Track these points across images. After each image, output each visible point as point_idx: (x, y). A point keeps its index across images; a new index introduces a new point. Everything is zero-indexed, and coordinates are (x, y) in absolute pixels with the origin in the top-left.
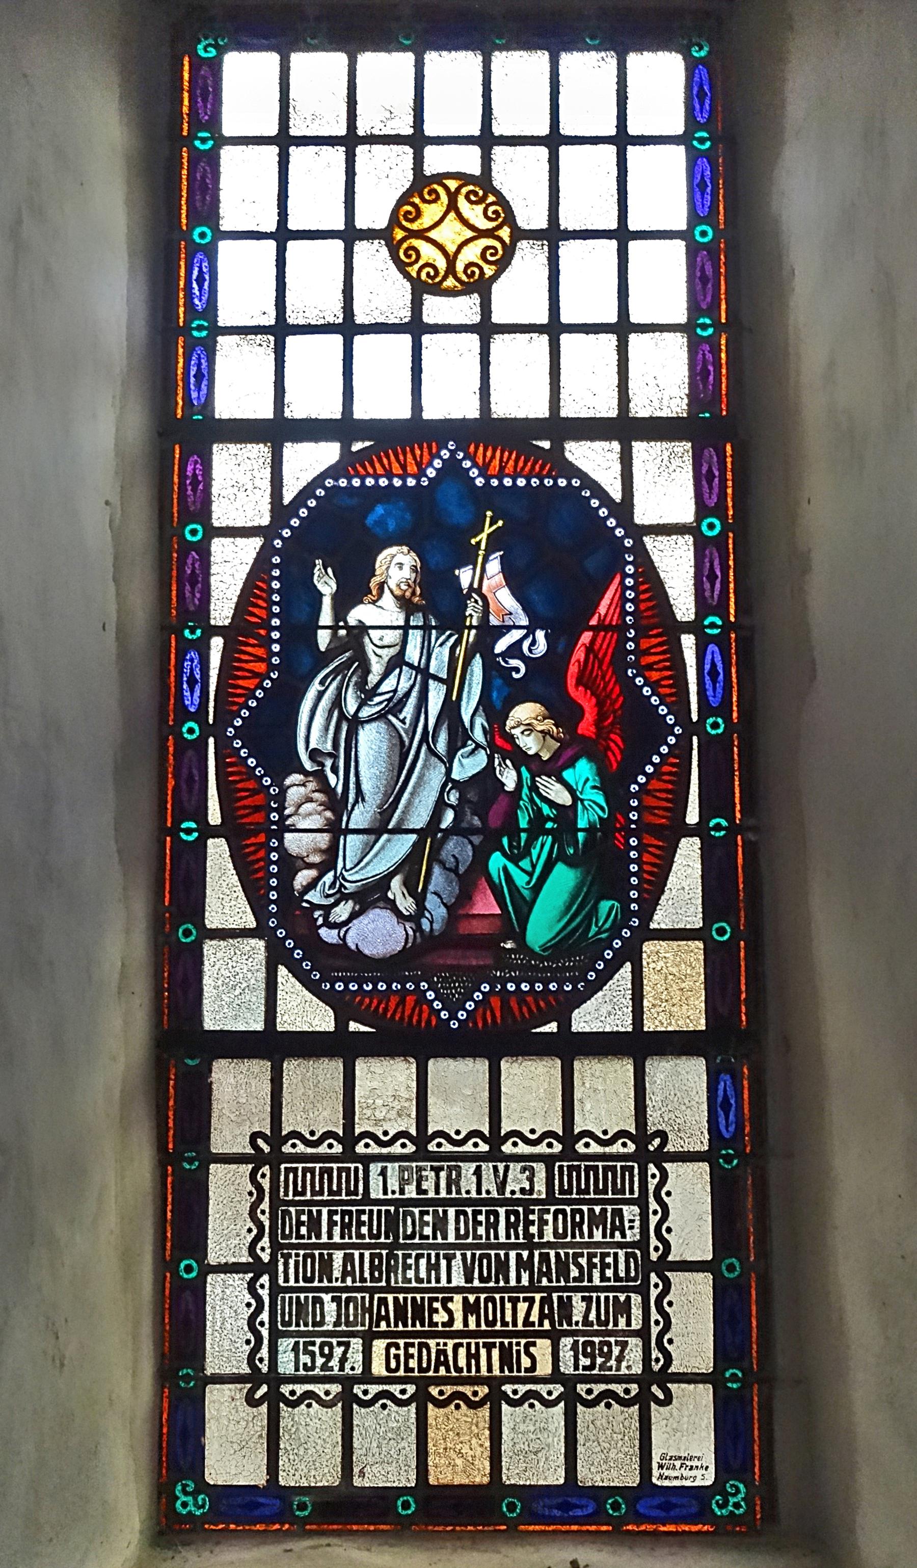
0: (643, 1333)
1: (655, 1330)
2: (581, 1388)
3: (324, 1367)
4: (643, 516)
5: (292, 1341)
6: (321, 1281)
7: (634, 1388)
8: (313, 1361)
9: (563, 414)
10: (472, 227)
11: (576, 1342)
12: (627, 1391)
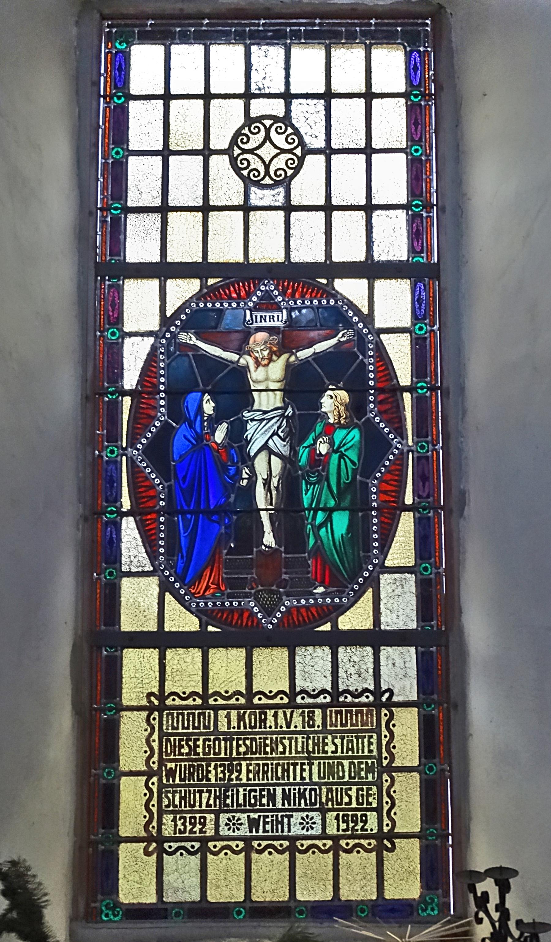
0: (379, 810)
1: (386, 808)
2: (343, 843)
3: (191, 831)
4: (379, 323)
5: (335, 814)
6: (189, 781)
7: (374, 842)
8: (348, 826)
9: (169, 260)
10: (276, 147)
11: (338, 815)
12: (324, 845)
